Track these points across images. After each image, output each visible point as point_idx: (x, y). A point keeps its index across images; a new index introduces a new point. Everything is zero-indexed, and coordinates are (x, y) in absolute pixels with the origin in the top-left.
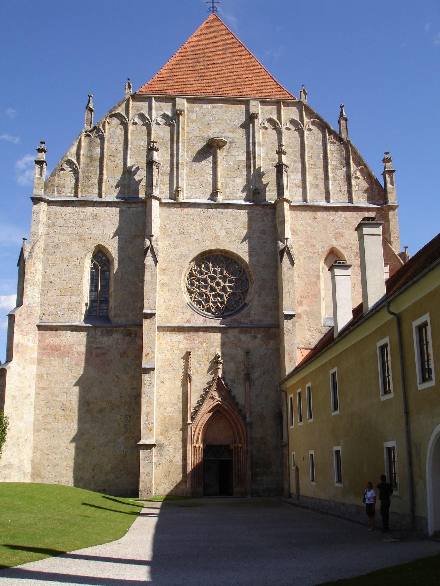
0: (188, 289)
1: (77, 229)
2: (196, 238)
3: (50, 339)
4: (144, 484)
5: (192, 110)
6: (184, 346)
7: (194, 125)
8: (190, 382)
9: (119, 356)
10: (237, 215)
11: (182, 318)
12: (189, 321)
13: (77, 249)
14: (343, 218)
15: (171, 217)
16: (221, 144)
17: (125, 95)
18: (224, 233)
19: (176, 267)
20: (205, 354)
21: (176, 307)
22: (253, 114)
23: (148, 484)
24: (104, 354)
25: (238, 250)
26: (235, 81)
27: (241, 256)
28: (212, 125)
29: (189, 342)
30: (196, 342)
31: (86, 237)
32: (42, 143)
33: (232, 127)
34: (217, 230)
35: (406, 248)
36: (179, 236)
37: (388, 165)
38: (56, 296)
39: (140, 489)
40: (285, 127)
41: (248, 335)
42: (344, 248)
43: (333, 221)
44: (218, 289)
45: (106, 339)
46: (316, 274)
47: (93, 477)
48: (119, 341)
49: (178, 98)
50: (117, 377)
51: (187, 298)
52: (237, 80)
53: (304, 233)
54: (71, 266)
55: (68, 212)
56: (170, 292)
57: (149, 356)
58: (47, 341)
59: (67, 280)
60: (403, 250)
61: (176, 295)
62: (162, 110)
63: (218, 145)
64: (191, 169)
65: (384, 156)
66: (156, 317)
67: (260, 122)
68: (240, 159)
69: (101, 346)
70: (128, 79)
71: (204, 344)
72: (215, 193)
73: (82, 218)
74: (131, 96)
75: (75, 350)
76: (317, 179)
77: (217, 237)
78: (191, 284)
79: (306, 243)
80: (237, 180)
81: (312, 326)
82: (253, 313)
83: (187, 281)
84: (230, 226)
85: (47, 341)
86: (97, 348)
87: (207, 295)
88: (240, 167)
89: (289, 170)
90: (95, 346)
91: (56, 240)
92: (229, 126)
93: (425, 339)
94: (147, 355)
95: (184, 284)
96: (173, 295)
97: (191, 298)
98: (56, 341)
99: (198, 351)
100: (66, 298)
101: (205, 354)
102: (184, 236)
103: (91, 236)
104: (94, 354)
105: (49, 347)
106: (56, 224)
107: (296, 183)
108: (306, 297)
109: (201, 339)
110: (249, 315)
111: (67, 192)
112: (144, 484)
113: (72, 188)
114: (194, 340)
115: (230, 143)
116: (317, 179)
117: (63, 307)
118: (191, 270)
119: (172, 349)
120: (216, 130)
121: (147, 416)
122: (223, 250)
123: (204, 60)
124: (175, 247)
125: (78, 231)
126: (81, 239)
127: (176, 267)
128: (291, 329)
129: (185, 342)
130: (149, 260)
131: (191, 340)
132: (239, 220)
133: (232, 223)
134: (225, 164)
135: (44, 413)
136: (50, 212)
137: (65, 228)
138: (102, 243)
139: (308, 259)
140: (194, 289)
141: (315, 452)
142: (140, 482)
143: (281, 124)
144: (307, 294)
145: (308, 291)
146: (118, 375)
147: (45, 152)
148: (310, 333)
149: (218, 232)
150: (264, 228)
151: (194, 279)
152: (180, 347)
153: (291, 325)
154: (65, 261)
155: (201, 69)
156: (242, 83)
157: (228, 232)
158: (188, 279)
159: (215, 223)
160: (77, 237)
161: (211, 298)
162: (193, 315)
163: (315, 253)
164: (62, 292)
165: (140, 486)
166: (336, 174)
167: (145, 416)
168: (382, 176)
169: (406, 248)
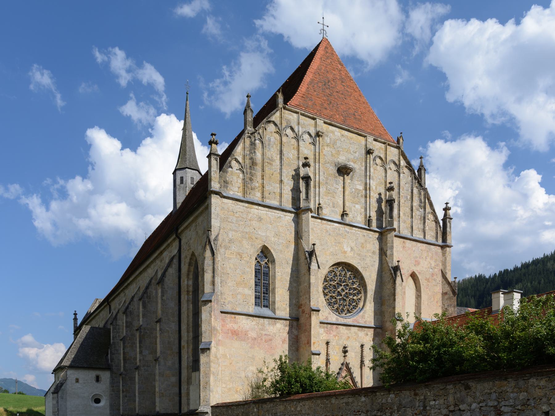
3: (231, 325)
9: (281, 343)
13: (247, 247)
17: (506, 146)
18: (349, 249)
24: (271, 340)
30: (331, 335)
32: (212, 135)
34: (345, 247)
35: (455, 278)
41: (363, 333)
42: (419, 273)
45: (272, 328)
54: (243, 262)
55: (238, 210)
58: (228, 326)
65: (444, 206)
69: (268, 333)
75: (249, 335)
77: (345, 252)
80: (357, 206)
82: (366, 316)
84: (353, 245)
85: (228, 326)
86: (265, 335)
92: (352, 157)
93: (115, 295)
94: (314, 343)
100: (240, 290)
106: (229, 220)
110: (363, 317)
113: (239, 188)
120: (344, 158)
129: (324, 335)
135: (228, 386)
137: (237, 225)
154: (238, 256)
160: (247, 236)
164: (238, 284)
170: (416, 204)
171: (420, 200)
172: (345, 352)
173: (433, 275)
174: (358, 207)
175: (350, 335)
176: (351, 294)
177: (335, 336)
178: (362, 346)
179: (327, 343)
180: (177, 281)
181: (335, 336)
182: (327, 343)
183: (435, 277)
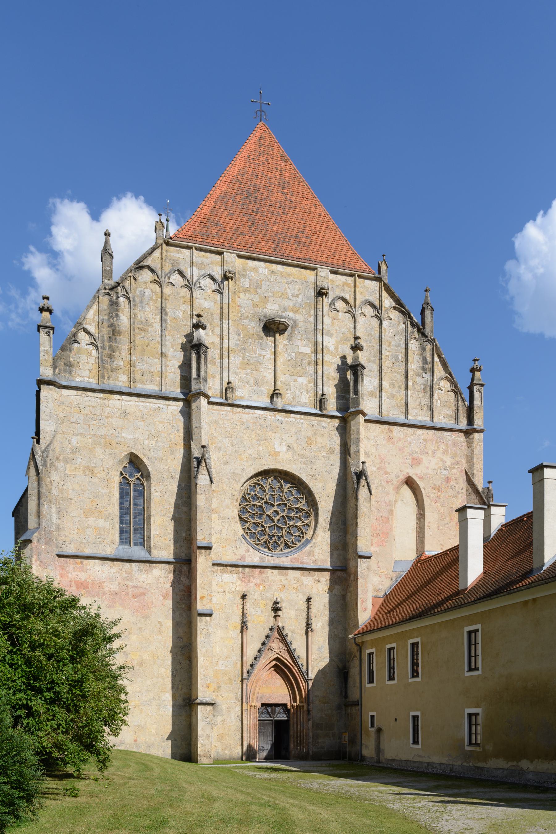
0: (240, 517)
1: (100, 429)
2: (251, 452)
3: (74, 574)
4: (203, 748)
5: (244, 273)
6: (237, 589)
7: (248, 296)
8: (246, 632)
9: (161, 598)
10: (300, 426)
11: (235, 554)
12: (243, 557)
14: (421, 441)
15: (220, 422)
16: (282, 327)
18: (284, 448)
19: (227, 488)
20: (262, 599)
21: (227, 540)
22: (322, 289)
23: (207, 747)
24: (143, 594)
25: (301, 472)
26: (297, 237)
27: (304, 480)
28: (269, 299)
29: (243, 584)
31: (113, 442)
33: (295, 304)
36: (230, 449)
37: (477, 374)
38: (79, 519)
39: (199, 753)
40: (360, 311)
41: (311, 578)
42: (421, 478)
43: (410, 443)
44: (276, 519)
45: (144, 575)
46: (388, 508)
47: (135, 741)
48: (161, 579)
49: (227, 252)
50: (159, 622)
51: (238, 528)
52: (301, 235)
53: (377, 456)
55: (88, 404)
56: (221, 521)
57: (205, 599)
59: (91, 497)
60: (487, 485)
61: (227, 525)
62: (204, 269)
63: (278, 328)
64: (243, 358)
65: (471, 364)
66: (213, 552)
67: (330, 301)
68: (304, 352)
69: (138, 584)
70: (384, 255)
71: (261, 587)
72: (275, 394)
73: (106, 414)
74: (165, 241)
75: (106, 589)
76: (394, 387)
77: (276, 454)
78: (243, 510)
79: (378, 468)
80: (300, 380)
81: (382, 570)
82: (317, 551)
83: (238, 508)
87: (263, 526)
88: (304, 362)
89: (365, 372)
90: (131, 584)
91: (74, 443)
94: (202, 598)
95: (234, 511)
96: (223, 525)
97: (244, 529)
98: (83, 577)
99: (254, 595)
100: (91, 521)
101: (262, 599)
102: (237, 449)
103: (120, 439)
104: (131, 594)
105: (73, 583)
106: (73, 420)
107: (369, 390)
108: (377, 535)
109: (258, 581)
110: (311, 553)
111: (83, 375)
112: (203, 748)
114: (249, 581)
115: (292, 327)
116: (394, 387)
117: (88, 533)
118: (244, 494)
119: (224, 592)
120: (276, 307)
121: (204, 671)
122: (283, 470)
123: (256, 197)
124: (225, 463)
125: (102, 432)
126: (108, 444)
127: (227, 488)
128: (365, 574)
129: (239, 583)
130: (363, 492)
131: (246, 581)
132: (303, 433)
133: (293, 436)
134: (286, 356)
136: (63, 403)
137: (85, 426)
138: (134, 451)
139: (380, 488)
140: (247, 518)
141: (422, 714)
142: (199, 746)
143: (355, 307)
144: (378, 532)
145: (378, 529)
146: (161, 620)
147: (51, 314)
148: (379, 579)
149: (277, 448)
150: (331, 446)
151: (247, 505)
152: (233, 589)
153: (366, 568)
155: (253, 211)
156: (307, 240)
157: (289, 447)
158: (240, 505)
159: (274, 434)
160: (102, 441)
161: (267, 530)
162: (248, 551)
163: (388, 482)
164: (88, 513)
165: (199, 750)
166: (418, 381)
167: (202, 670)
168: (468, 390)
169: (490, 482)
170: (415, 364)
171: (425, 361)
172: (276, 609)
173: (448, 480)
174: (302, 380)
175: (286, 583)
176: (290, 518)
177: (258, 585)
178: (308, 600)
179: (244, 597)
180: (110, 563)
181: (258, 585)
182: (244, 597)
183: (453, 483)
